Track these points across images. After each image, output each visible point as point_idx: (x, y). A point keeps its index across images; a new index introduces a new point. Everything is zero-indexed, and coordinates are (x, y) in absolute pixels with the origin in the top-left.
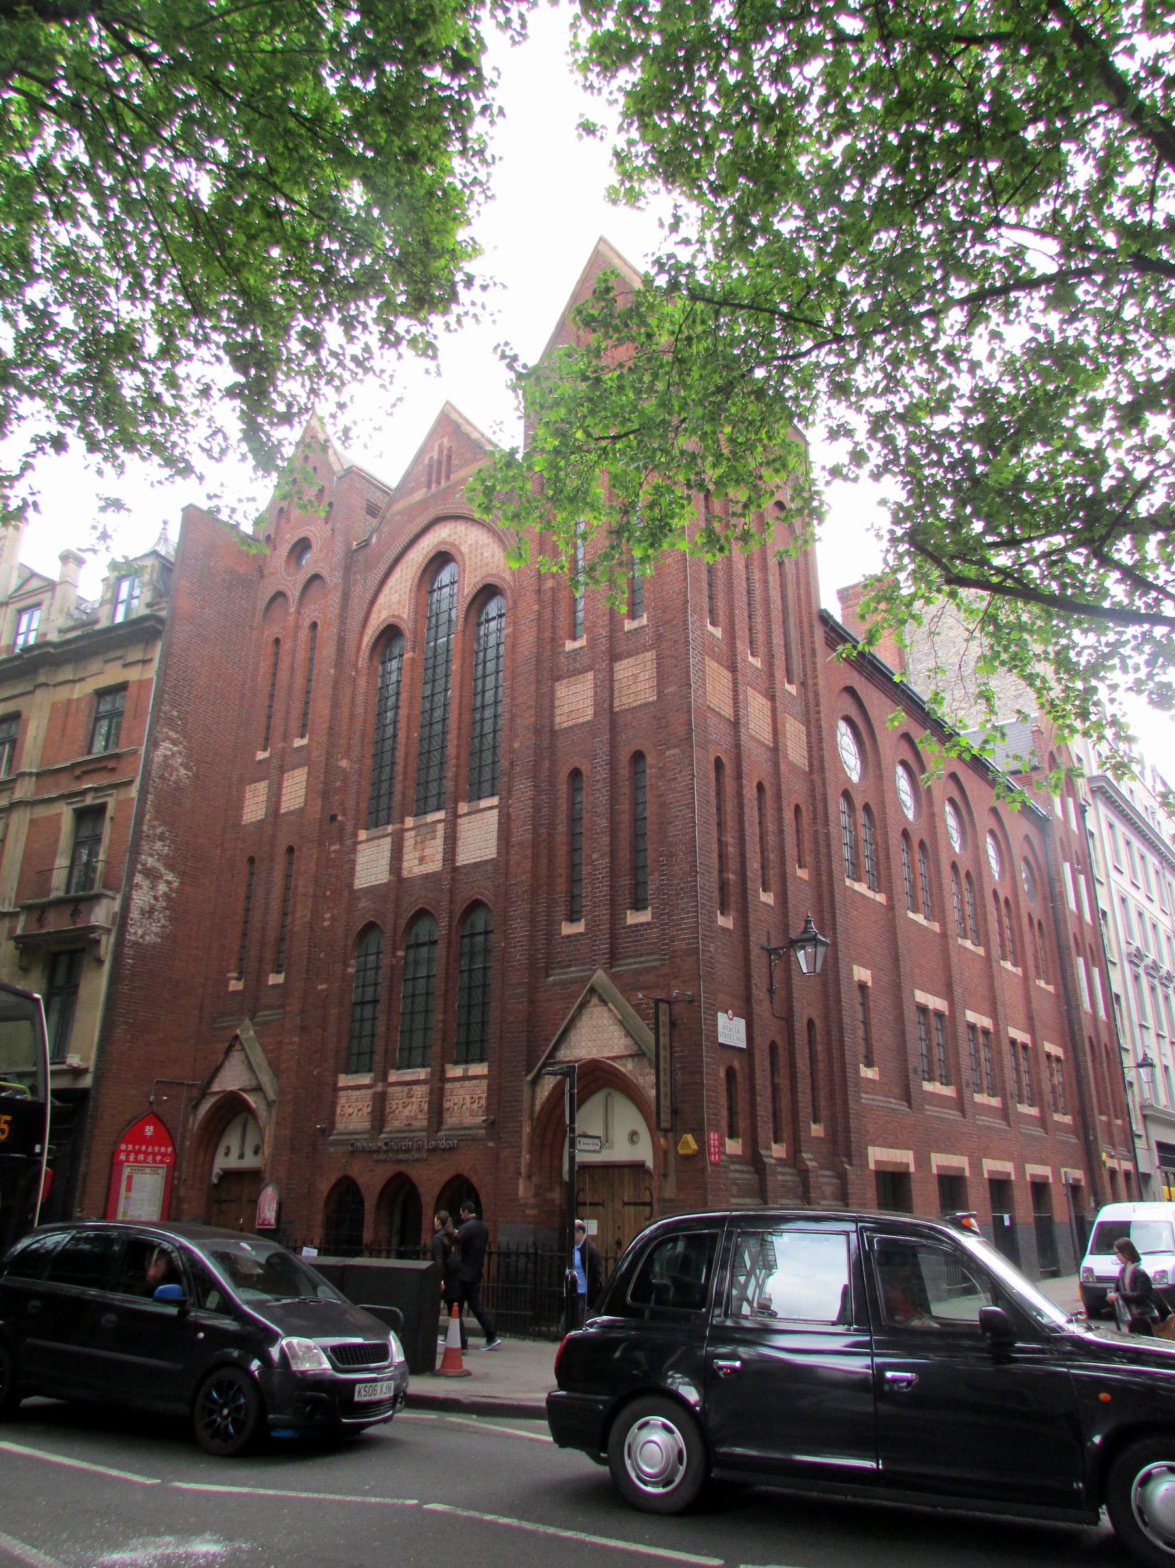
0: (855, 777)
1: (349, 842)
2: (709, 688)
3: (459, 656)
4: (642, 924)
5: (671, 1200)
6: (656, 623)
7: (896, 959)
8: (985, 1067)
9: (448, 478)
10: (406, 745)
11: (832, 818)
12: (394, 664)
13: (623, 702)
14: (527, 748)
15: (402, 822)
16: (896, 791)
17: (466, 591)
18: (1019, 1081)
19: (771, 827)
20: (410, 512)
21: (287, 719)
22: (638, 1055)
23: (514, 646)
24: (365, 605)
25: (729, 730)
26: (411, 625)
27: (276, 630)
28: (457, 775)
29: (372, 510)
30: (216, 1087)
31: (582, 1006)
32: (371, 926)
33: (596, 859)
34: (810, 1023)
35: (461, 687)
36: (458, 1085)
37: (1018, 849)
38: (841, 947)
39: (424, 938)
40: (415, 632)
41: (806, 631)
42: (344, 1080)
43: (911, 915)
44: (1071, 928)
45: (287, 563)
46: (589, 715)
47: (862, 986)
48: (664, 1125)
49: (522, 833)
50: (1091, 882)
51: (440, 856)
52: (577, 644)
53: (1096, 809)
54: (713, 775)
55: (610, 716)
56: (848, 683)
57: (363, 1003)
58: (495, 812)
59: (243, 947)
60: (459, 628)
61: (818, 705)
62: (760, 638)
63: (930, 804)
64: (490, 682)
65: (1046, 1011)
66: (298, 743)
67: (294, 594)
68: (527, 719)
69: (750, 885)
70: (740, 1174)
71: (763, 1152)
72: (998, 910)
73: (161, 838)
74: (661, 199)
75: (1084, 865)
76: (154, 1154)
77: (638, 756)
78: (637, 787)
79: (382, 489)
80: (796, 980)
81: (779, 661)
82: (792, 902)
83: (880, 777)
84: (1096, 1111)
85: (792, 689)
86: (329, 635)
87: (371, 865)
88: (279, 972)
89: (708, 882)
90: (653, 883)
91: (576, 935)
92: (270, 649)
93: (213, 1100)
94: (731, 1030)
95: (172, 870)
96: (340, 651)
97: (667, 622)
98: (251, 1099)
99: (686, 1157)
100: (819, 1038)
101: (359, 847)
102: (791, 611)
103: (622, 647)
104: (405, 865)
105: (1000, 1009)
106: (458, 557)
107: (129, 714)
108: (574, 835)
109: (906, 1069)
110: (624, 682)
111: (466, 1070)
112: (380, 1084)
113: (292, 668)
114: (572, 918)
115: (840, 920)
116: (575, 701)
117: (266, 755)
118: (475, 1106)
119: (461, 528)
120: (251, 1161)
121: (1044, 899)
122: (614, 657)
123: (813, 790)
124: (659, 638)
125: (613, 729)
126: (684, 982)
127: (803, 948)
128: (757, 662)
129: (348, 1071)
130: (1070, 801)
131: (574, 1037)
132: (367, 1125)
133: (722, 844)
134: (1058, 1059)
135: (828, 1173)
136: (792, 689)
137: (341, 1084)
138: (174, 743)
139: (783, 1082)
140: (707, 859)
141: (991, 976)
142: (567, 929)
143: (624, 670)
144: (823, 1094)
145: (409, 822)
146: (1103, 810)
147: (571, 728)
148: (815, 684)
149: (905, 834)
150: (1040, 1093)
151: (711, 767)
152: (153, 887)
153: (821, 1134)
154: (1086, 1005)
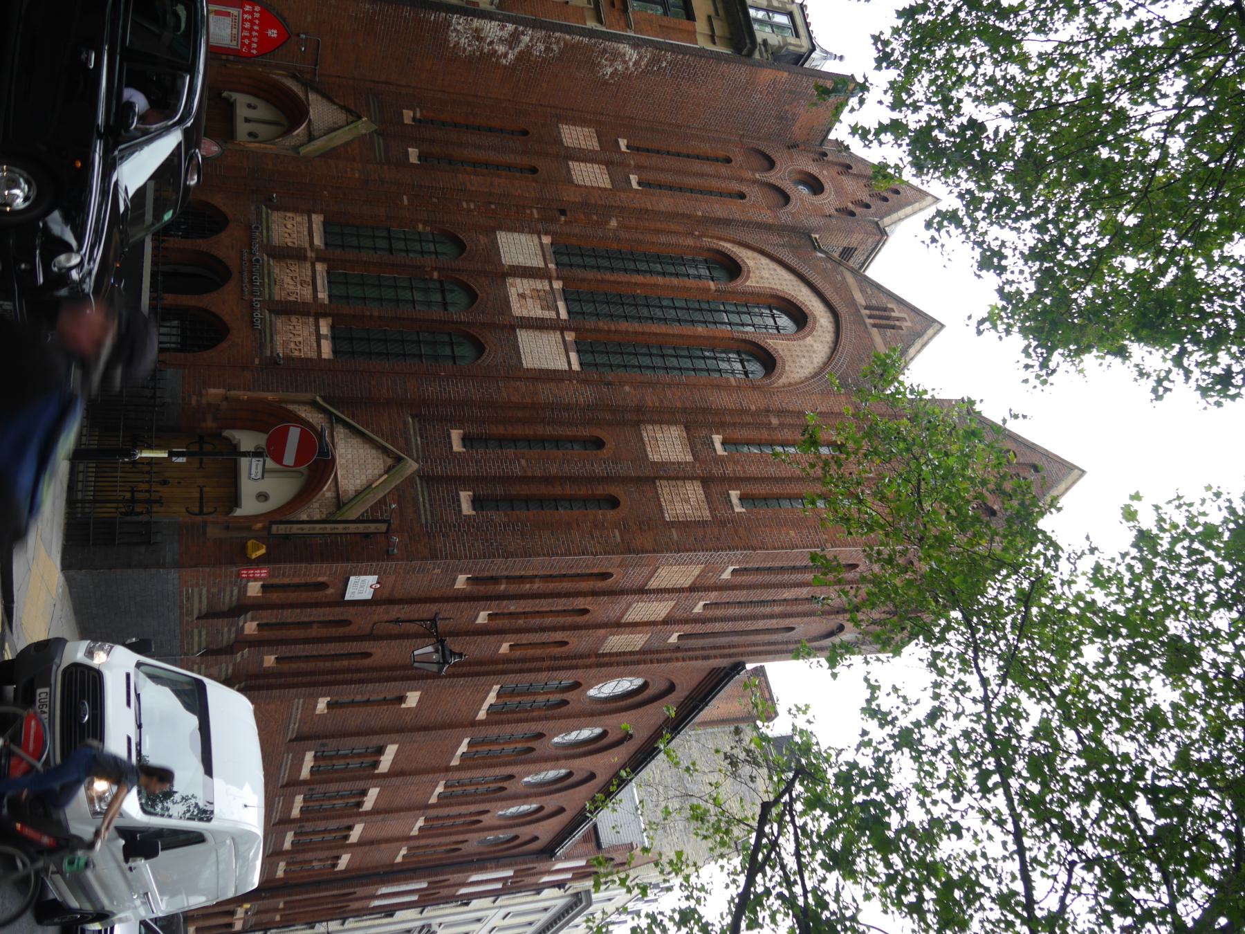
0: (592, 692)
1: (540, 226)
2: (675, 568)
3: (711, 334)
4: (459, 506)
5: (204, 533)
6: (736, 520)
7: (426, 728)
8: (327, 804)
9: (874, 326)
10: (629, 283)
11: (555, 674)
12: (704, 272)
13: (665, 490)
14: (624, 399)
15: (558, 278)
16: (580, 728)
17: (770, 341)
18: (315, 832)
19: (548, 621)
20: (843, 288)
21: (657, 169)
22: (339, 503)
23: (718, 386)
24: (760, 245)
25: (636, 585)
26: (740, 288)
27: (738, 158)
28: (600, 331)
29: (847, 252)
30: (312, 97)
31: (385, 451)
32: (461, 246)
33: (520, 463)
34: (368, 655)
35: (681, 336)
36: (312, 329)
37: (526, 832)
38: (437, 682)
39: (449, 297)
40: (733, 293)
41: (726, 651)
42: (317, 219)
43: (466, 741)
44: (455, 878)
45: (801, 172)
46: (654, 457)
47: (402, 699)
48: (274, 529)
49: (546, 393)
50: (496, 894)
51: (525, 313)
52: (718, 446)
53: (562, 897)
54: (596, 571)
55: (656, 476)
56: (678, 688)
57: (389, 238)
58: (567, 368)
59: (444, 124)
60: (736, 335)
61: (659, 661)
62: (720, 612)
63: (567, 757)
64: (687, 363)
65: (378, 856)
66: (634, 179)
67: (773, 177)
68: (651, 399)
69: (494, 603)
70: (229, 598)
71: (249, 615)
72: (471, 814)
73: (548, 49)
74: (1116, 543)
75: (511, 888)
76: (250, 38)
77: (614, 503)
78: (585, 501)
79: (866, 263)
80: (406, 643)
81: (699, 628)
82: (479, 639)
83: (592, 714)
84: (288, 899)
85: (673, 639)
86: (731, 209)
87: (518, 248)
88: (420, 158)
89: (497, 566)
90: (498, 516)
91: (450, 443)
92: (721, 153)
93: (301, 94)
94: (361, 587)
95: (517, 59)
96: (718, 221)
97: (736, 532)
98: (301, 130)
99: (244, 548)
100: (354, 662)
101: (535, 237)
102: (744, 638)
103: (715, 489)
104: (518, 280)
105: (380, 817)
106: (801, 334)
107: (666, 21)
108: (542, 441)
109: (326, 737)
110: (682, 490)
111: (326, 337)
112: (313, 255)
113: (702, 175)
114: (465, 440)
115: (462, 681)
116: (667, 445)
117: (623, 148)
118: (292, 345)
119: (829, 337)
120: (242, 129)
121: (480, 854)
122: (706, 481)
123: (581, 657)
124: (722, 523)
125: (639, 480)
126: (406, 545)
127: (437, 651)
128: (698, 609)
129: (325, 224)
130: (569, 876)
131: (356, 442)
132: (276, 240)
133: (532, 579)
134: (335, 865)
135: (230, 670)
136: (673, 639)
137: (314, 216)
138: (636, 63)
139: (314, 632)
140: (518, 567)
141: (409, 809)
142: (456, 435)
143: (694, 491)
144: (303, 666)
145: (557, 285)
146: (561, 903)
147: (642, 439)
148: (677, 659)
149: (540, 736)
150: (304, 851)
151: (603, 570)
152: (501, 40)
153: (266, 664)
154: (384, 890)
